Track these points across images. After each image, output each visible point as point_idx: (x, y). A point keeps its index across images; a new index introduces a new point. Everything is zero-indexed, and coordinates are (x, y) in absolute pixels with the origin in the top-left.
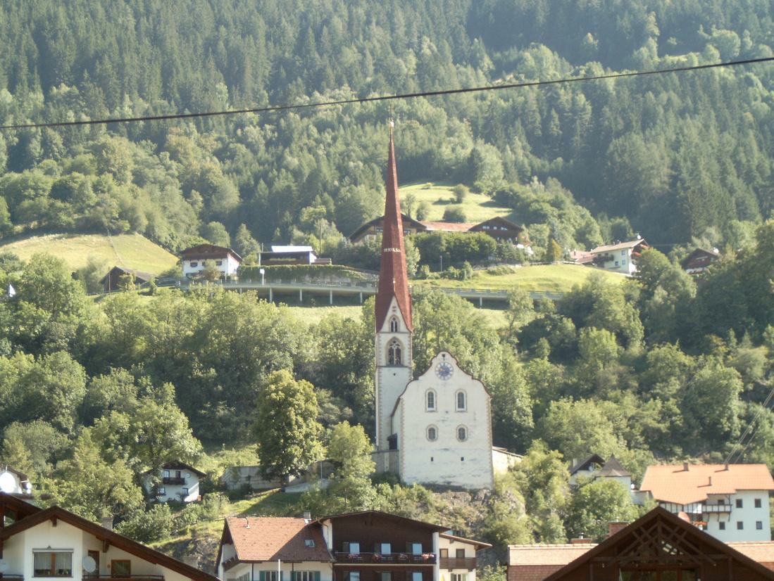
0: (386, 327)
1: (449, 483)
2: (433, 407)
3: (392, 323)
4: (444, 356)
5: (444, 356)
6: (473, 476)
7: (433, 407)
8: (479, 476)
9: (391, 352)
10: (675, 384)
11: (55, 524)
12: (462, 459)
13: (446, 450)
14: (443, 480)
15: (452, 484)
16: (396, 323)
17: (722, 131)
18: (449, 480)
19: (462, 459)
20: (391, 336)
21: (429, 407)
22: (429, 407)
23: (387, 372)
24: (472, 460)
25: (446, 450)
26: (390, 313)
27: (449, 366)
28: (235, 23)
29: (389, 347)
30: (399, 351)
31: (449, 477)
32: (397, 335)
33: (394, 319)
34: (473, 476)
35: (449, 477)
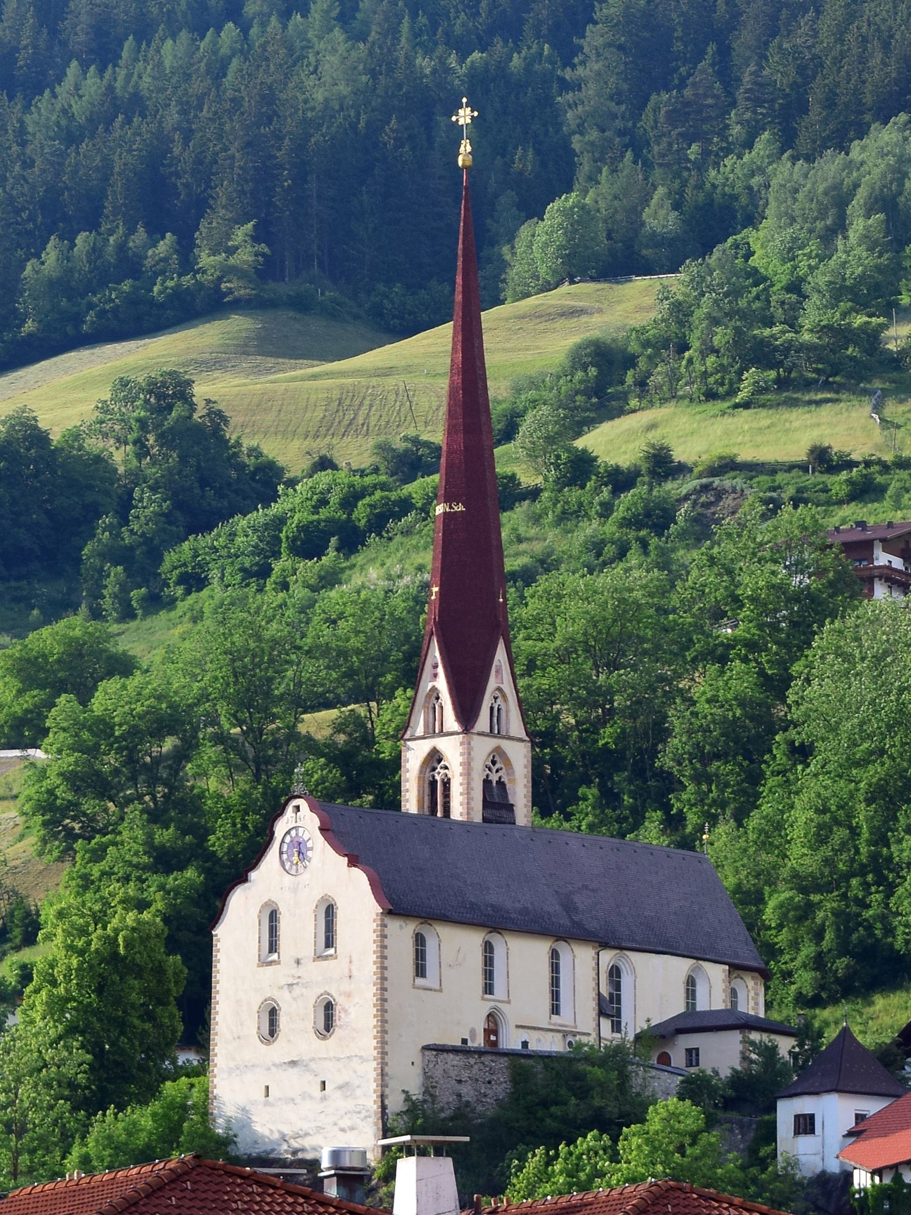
3: (492, 709)
6: (343, 1130)
8: (352, 1128)
13: (293, 1063)
16: (499, 710)
25: (293, 1063)
34: (343, 1130)
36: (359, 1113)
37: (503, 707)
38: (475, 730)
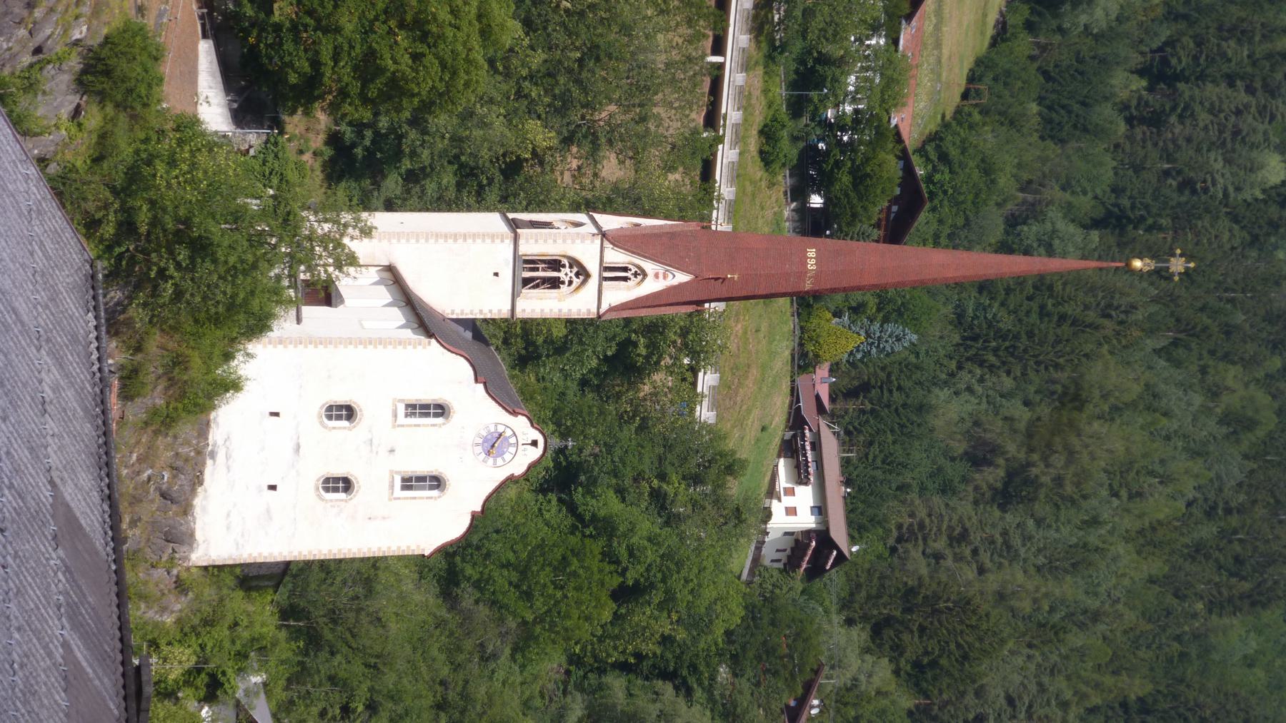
0: (616, 257)
1: (213, 455)
2: (405, 488)
3: (625, 269)
4: (534, 443)
5: (534, 443)
6: (228, 515)
7: (405, 488)
9: (555, 264)
10: (426, 696)
11: (234, 385)
12: (273, 488)
13: (298, 448)
14: (220, 442)
15: (209, 462)
16: (625, 279)
17: (1099, 523)
18: (221, 457)
19: (273, 488)
20: (593, 267)
21: (408, 406)
22: (404, 480)
23: (502, 255)
24: (268, 511)
25: (298, 448)
26: (649, 266)
27: (508, 457)
28: (1206, 230)
29: (565, 261)
30: (555, 283)
31: (228, 457)
32: (593, 282)
33: (636, 275)
34: (228, 515)
35: (228, 457)
36: (243, 535)
37: (630, 283)
38: (606, 244)
